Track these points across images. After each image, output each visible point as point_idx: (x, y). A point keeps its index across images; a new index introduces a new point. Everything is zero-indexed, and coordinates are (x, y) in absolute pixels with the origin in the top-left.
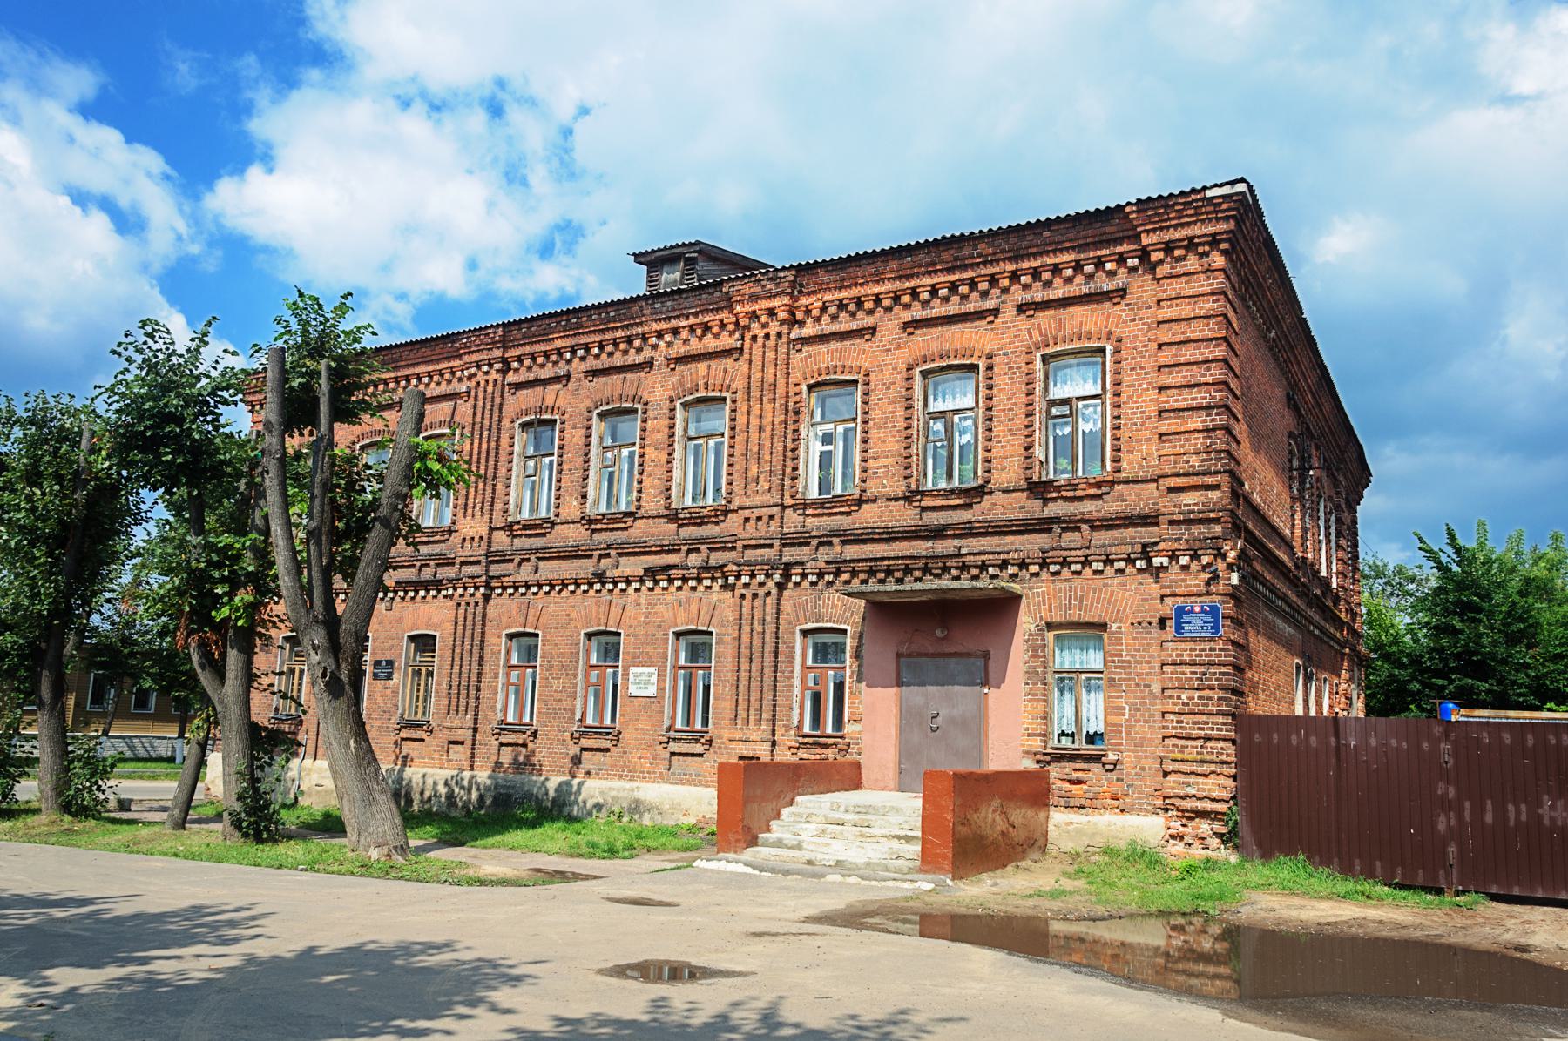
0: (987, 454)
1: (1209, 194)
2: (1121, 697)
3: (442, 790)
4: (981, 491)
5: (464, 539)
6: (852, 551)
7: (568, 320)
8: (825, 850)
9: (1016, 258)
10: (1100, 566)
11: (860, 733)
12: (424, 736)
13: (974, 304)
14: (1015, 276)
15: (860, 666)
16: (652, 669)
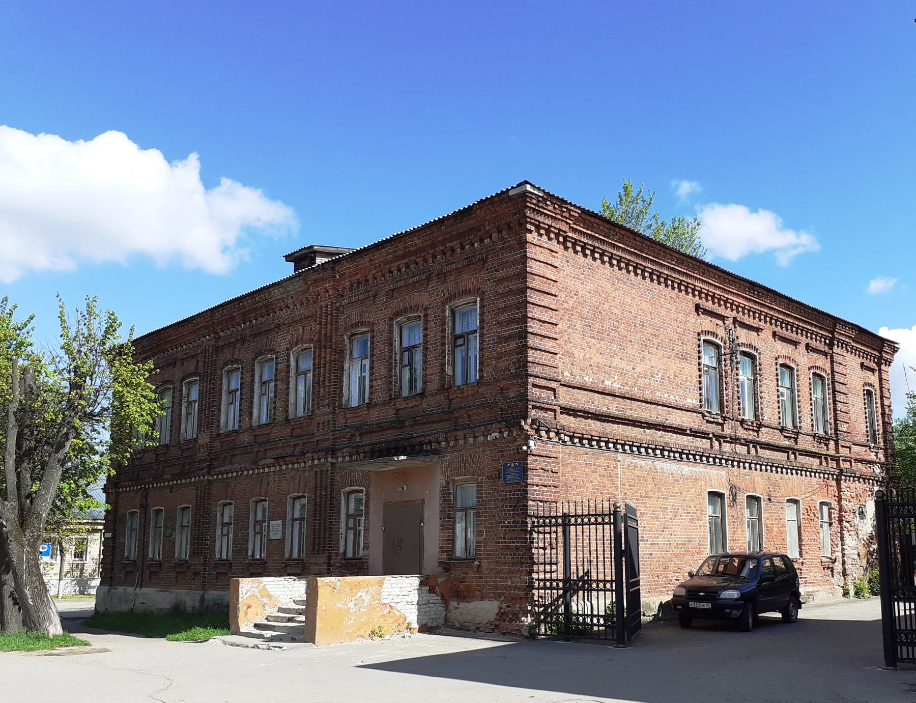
1: (511, 193)
2: (482, 524)
5: (319, 424)
16: (280, 522)
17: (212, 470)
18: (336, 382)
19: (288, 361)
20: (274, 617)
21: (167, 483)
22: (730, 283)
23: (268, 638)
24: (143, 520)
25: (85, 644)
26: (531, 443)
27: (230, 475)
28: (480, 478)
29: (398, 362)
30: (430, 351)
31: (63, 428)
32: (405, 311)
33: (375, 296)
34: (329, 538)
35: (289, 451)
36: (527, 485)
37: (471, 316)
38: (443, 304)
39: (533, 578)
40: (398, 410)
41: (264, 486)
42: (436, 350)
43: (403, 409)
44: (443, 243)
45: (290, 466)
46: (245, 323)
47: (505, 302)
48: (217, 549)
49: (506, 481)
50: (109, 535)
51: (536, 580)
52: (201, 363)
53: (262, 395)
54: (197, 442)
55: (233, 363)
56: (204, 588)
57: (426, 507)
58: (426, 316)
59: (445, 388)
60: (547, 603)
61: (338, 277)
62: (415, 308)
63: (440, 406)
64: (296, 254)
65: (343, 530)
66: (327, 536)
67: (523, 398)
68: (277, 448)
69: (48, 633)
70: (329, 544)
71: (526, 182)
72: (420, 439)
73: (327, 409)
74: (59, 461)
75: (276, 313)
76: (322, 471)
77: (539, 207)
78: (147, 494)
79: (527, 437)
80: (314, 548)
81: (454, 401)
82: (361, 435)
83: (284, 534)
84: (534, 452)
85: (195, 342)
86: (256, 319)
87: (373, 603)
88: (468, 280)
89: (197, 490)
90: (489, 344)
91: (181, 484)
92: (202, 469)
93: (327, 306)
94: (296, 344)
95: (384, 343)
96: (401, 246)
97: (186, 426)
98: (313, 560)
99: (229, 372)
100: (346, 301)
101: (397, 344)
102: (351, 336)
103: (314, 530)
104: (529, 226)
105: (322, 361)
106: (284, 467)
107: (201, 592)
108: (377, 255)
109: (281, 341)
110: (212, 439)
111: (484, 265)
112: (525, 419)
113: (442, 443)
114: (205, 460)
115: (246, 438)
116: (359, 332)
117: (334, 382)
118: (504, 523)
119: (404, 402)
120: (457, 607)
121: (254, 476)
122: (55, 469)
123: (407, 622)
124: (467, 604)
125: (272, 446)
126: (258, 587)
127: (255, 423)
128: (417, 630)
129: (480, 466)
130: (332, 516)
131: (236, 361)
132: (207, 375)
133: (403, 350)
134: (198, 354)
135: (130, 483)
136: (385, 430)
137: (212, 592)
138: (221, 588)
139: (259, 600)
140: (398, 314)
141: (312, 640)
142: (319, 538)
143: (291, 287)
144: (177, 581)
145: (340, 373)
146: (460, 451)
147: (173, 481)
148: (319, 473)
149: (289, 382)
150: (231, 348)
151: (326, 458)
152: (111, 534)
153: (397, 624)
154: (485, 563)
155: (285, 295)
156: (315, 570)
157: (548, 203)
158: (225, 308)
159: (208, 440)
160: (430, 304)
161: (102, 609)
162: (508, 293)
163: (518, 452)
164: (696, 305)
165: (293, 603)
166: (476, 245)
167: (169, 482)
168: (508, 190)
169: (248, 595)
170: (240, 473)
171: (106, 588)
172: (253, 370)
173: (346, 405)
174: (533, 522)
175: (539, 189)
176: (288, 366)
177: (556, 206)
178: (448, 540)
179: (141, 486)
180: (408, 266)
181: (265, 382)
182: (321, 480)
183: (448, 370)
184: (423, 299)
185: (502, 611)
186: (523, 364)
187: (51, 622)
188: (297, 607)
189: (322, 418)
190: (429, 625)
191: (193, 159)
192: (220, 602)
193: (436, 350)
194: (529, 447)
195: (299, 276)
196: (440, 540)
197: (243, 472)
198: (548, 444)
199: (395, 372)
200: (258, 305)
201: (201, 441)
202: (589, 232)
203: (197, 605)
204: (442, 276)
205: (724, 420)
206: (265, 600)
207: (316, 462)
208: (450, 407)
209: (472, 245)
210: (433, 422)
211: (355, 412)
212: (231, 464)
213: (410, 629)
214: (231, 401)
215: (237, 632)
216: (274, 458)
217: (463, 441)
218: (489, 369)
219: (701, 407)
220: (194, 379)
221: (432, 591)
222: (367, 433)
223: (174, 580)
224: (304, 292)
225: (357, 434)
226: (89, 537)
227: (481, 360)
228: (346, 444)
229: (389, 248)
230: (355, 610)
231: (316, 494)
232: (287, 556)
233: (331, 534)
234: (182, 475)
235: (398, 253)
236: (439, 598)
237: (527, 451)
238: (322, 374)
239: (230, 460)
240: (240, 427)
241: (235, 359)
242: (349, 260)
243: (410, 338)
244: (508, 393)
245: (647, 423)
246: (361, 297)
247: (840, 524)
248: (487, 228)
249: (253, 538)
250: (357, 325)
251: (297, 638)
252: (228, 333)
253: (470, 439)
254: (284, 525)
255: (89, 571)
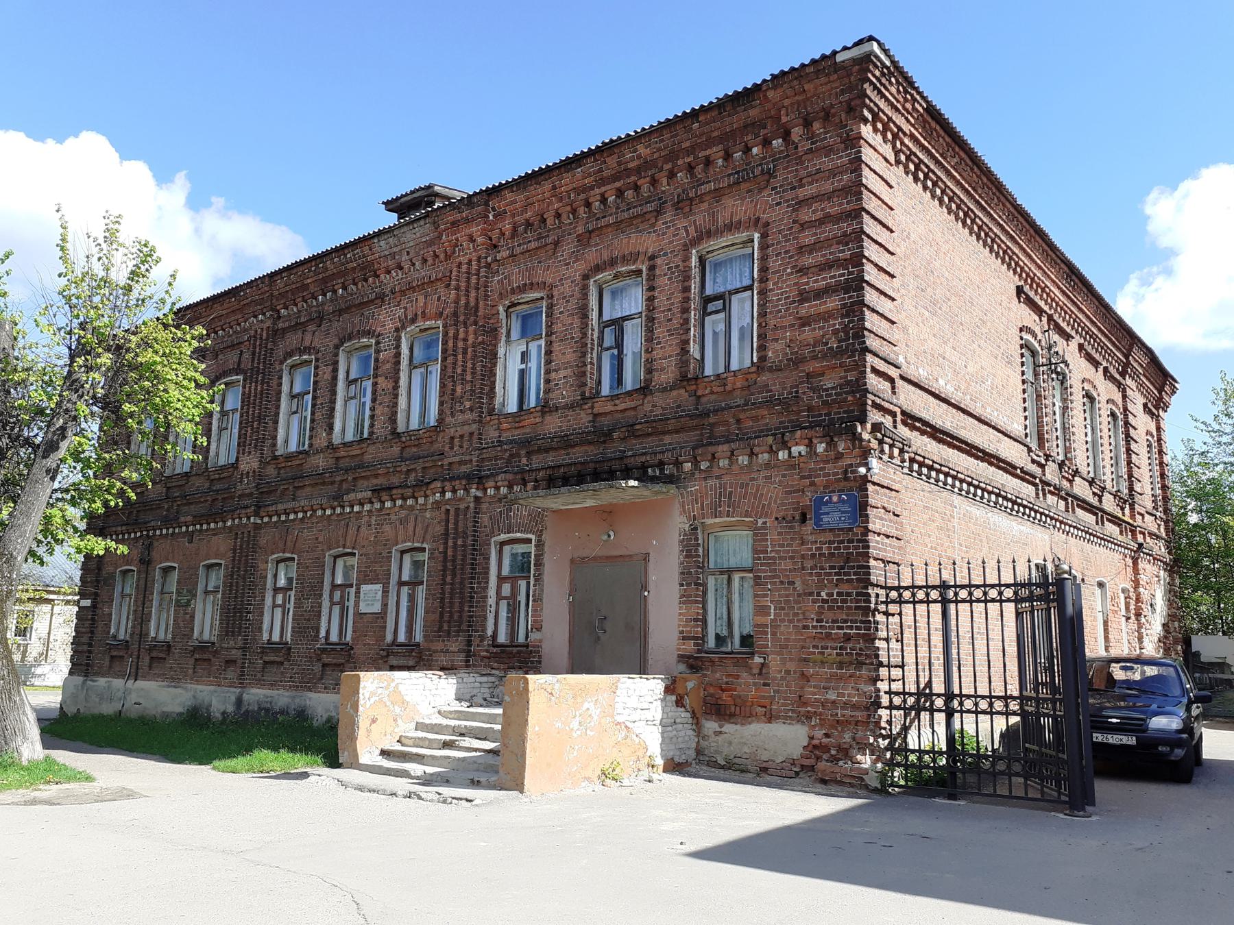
1: (839, 58)
2: (766, 596)
5: (452, 438)
16: (379, 587)
17: (262, 509)
18: (484, 375)
19: (398, 346)
20: (415, 738)
21: (184, 529)
22: (1054, 263)
23: (418, 778)
24: (142, 582)
25: (87, 779)
26: (874, 462)
27: (292, 517)
28: (760, 521)
29: (596, 342)
30: (659, 323)
31: (58, 419)
32: (612, 263)
33: (556, 243)
34: (470, 611)
35: (395, 480)
36: (867, 531)
37: (731, 267)
38: (686, 248)
39: (879, 690)
40: (595, 416)
41: (352, 532)
42: (671, 320)
43: (605, 414)
44: (691, 151)
45: (399, 502)
46: (324, 295)
47: (816, 234)
48: (266, 626)
49: (821, 526)
50: (87, 603)
51: (886, 693)
52: (246, 356)
53: (348, 399)
54: (237, 468)
55: (301, 353)
56: (242, 685)
57: (651, 566)
58: (652, 268)
59: (689, 378)
60: (894, 732)
61: (491, 218)
62: (633, 257)
63: (679, 407)
64: (403, 200)
65: (492, 601)
66: (466, 609)
67: (860, 388)
68: (376, 476)
69: (20, 755)
70: (469, 621)
71: (871, 38)
72: (643, 459)
73: (468, 416)
74: (48, 471)
75: (378, 276)
76: (457, 510)
77: (882, 84)
78: (150, 545)
79: (866, 453)
80: (441, 627)
81: (704, 400)
82: (529, 454)
83: (385, 605)
84: (875, 479)
85: (239, 324)
86: (344, 288)
87: (603, 720)
88: (735, 207)
89: (236, 539)
90: (778, 306)
91: (201, 530)
92: (246, 507)
93: (469, 262)
94: (413, 321)
95: (572, 314)
96: (612, 161)
97: (218, 447)
98: (439, 646)
99: (293, 367)
100: (504, 254)
101: (594, 315)
102: (509, 307)
103: (442, 599)
104: (866, 113)
105: (460, 344)
106: (388, 504)
107: (238, 690)
108: (567, 178)
109: (386, 319)
110: (263, 463)
111: (768, 181)
112: (863, 422)
113: (685, 464)
114: (251, 494)
115: (320, 462)
116: (524, 300)
117: (482, 375)
118: (819, 594)
119: (609, 403)
120: (721, 732)
121: (334, 518)
122: (42, 484)
123: (648, 754)
124: (738, 727)
125: (369, 473)
126: (387, 688)
127: (337, 439)
128: (661, 768)
129: (759, 502)
130: (473, 578)
131: (308, 350)
132: (258, 371)
133: (604, 325)
134: (242, 343)
135: (124, 528)
136: (573, 446)
137: (254, 691)
138: (272, 685)
139: (389, 711)
140: (598, 269)
141: (518, 786)
142: (450, 612)
143: (409, 236)
144: (194, 672)
145: (490, 362)
146: (718, 477)
147: (194, 525)
148: (452, 512)
149: (399, 378)
150: (300, 332)
151: (467, 490)
152: (89, 601)
153: (635, 758)
154: (774, 662)
155: (396, 249)
156: (442, 661)
157: (893, 80)
158: (295, 271)
159: (256, 465)
160: (660, 250)
161: (71, 710)
162: (821, 222)
163: (846, 479)
164: (1018, 287)
165: (438, 715)
166: (755, 150)
167: (187, 527)
168: (835, 53)
169: (372, 700)
170: (309, 514)
171: (79, 679)
172: (337, 362)
173: (500, 410)
174: (877, 595)
175: (886, 51)
176: (398, 355)
177: (901, 88)
178: (696, 620)
179: (142, 532)
180: (620, 193)
181: (355, 381)
182: (456, 523)
183: (694, 350)
184: (647, 242)
185: (816, 742)
186: (859, 332)
187: (25, 738)
188: (445, 722)
189: (458, 429)
190: (677, 760)
191: (181, 179)
192: (269, 706)
193: (671, 320)
194: (869, 470)
195: (428, 216)
196: (680, 620)
197: (314, 511)
198: (889, 467)
199: (592, 358)
200: (350, 266)
201: (244, 467)
202: (926, 144)
203: (230, 709)
204: (684, 204)
205: (1047, 460)
206: (397, 710)
207: (448, 495)
208: (697, 409)
209: (747, 150)
210: (664, 433)
211: (517, 419)
212: (293, 500)
213: (653, 766)
214: (294, 409)
215: (355, 764)
216: (373, 491)
217: (727, 462)
218: (780, 346)
219: (1026, 435)
220: (234, 378)
221: (679, 703)
222: (539, 451)
223: (190, 671)
224: (430, 243)
225: (523, 452)
226: (36, 609)
227: (762, 331)
228: (502, 468)
229: (590, 166)
230: (579, 732)
231: (446, 543)
232: (389, 638)
233: (472, 607)
234: (210, 517)
235: (606, 173)
236: (688, 715)
237: (866, 476)
238: (460, 363)
239: (293, 495)
240: (311, 445)
241: (305, 348)
242: (515, 189)
243: (613, 308)
244: (821, 381)
245: (983, 451)
246: (533, 245)
247: (1137, 620)
248: (784, 119)
249: (328, 610)
250: (522, 289)
251: (481, 780)
252: (295, 310)
253: (740, 458)
254: (385, 592)
255: (35, 654)
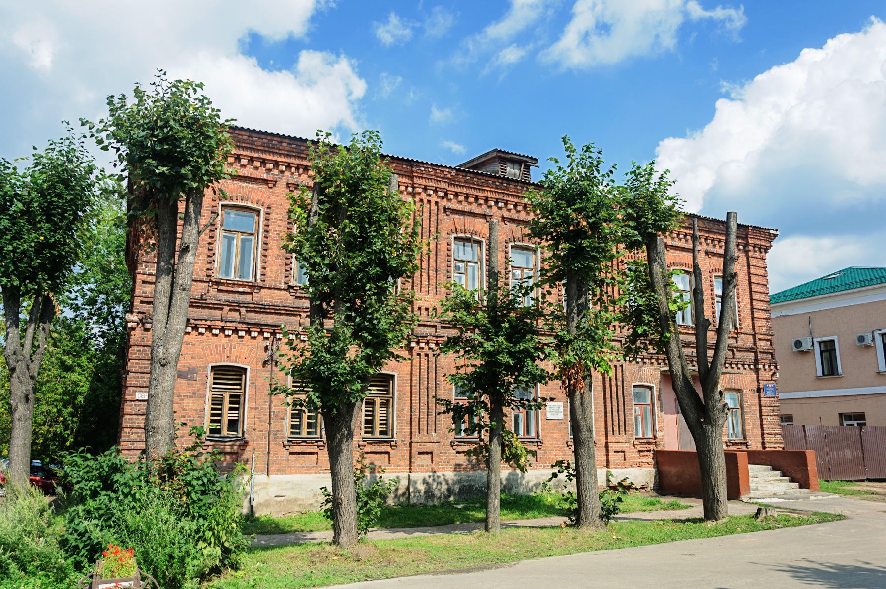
0: (263, 264)
3: (422, 487)
4: (255, 287)
6: (252, 317)
7: (502, 183)
8: (765, 489)
9: (709, 232)
10: (203, 331)
11: (663, 436)
12: (388, 449)
13: (262, 174)
14: (251, 160)
15: (661, 404)
